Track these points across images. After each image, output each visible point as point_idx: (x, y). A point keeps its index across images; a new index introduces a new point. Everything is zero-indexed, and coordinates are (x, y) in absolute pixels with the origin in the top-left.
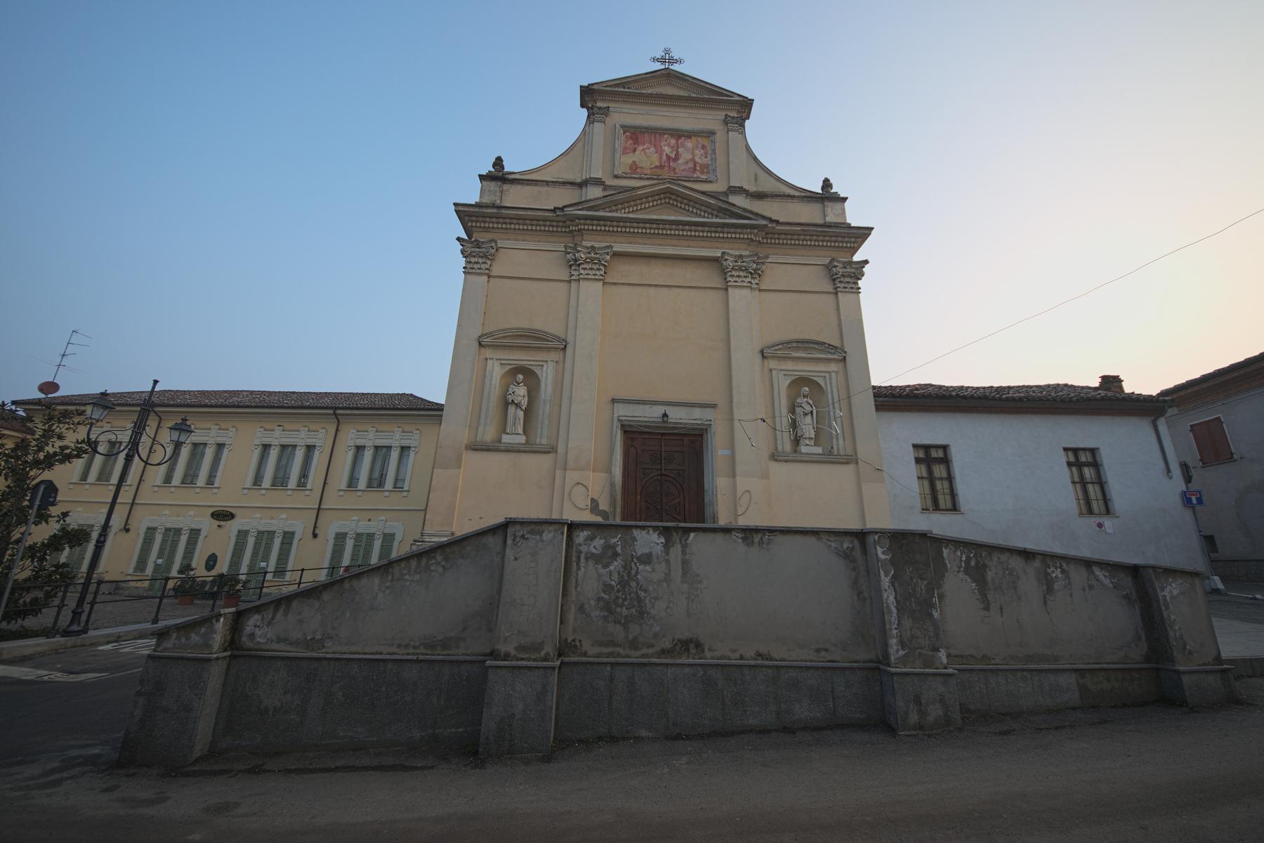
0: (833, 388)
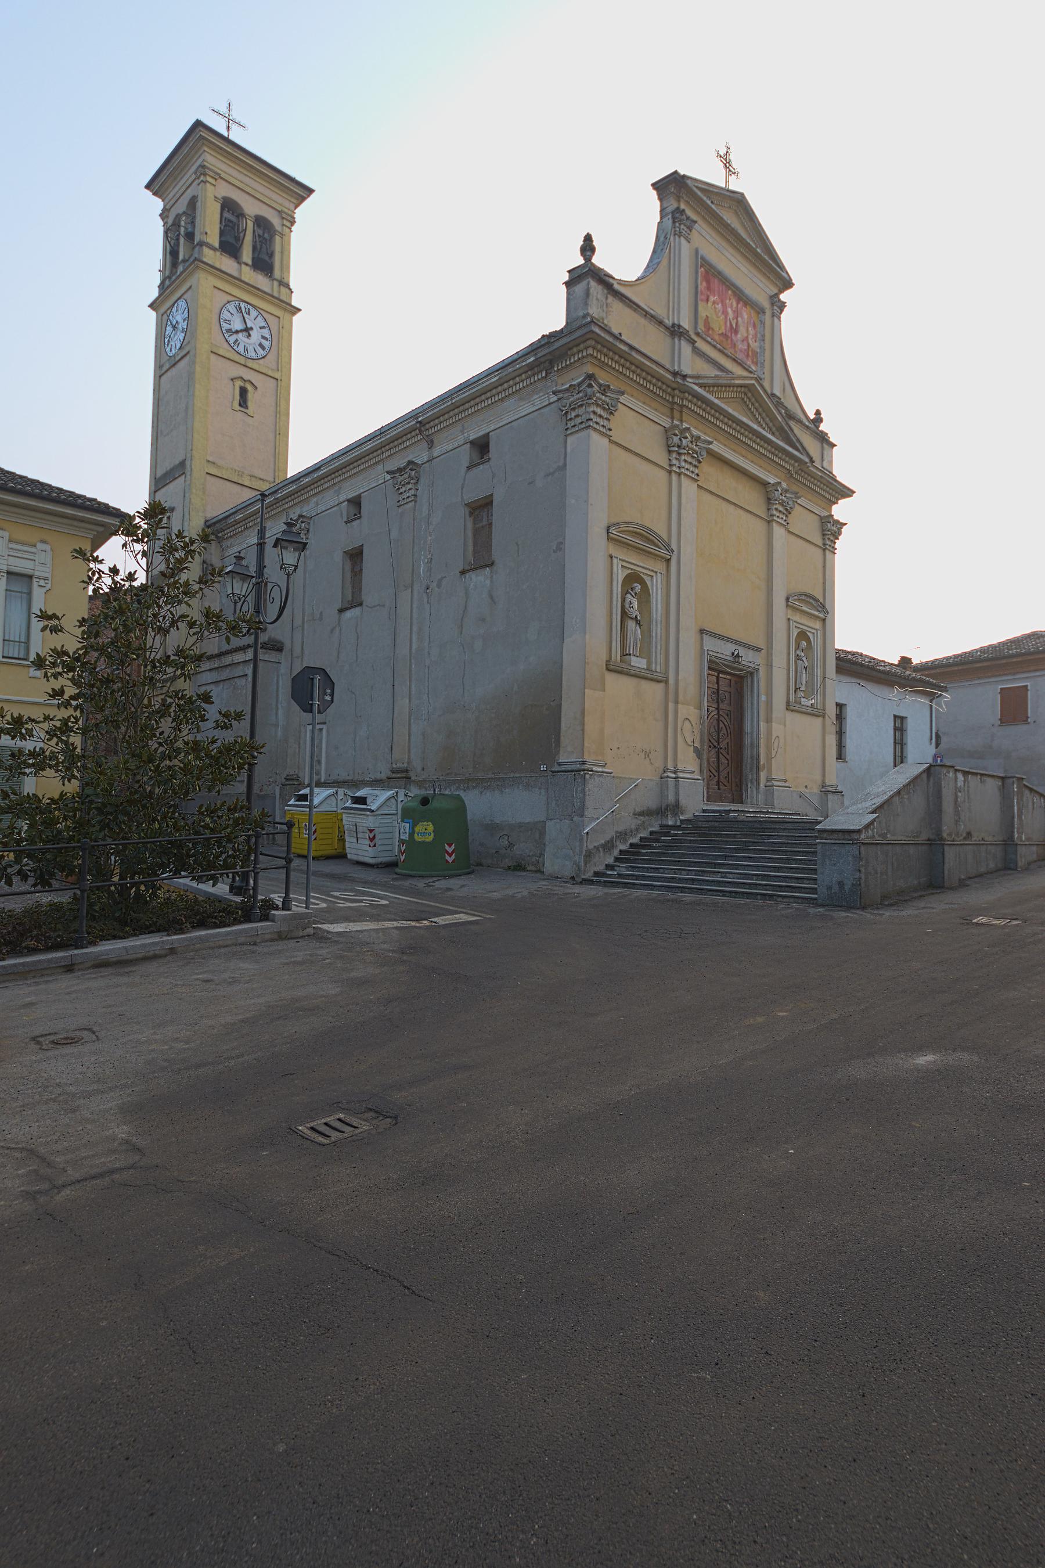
0: (817, 644)
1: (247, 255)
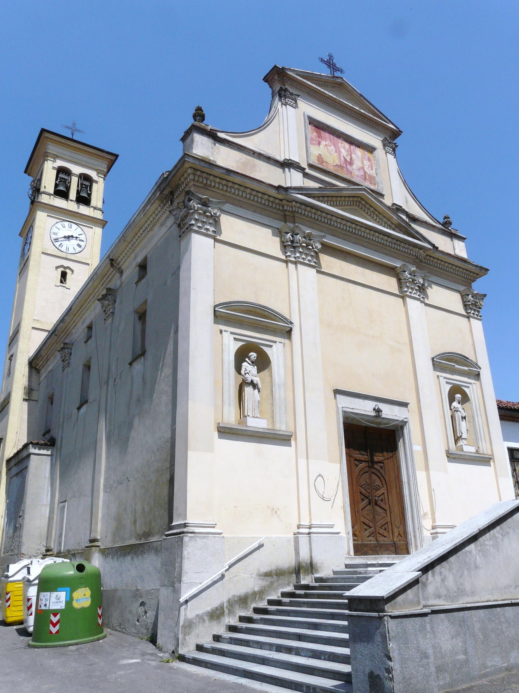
1: (73, 195)
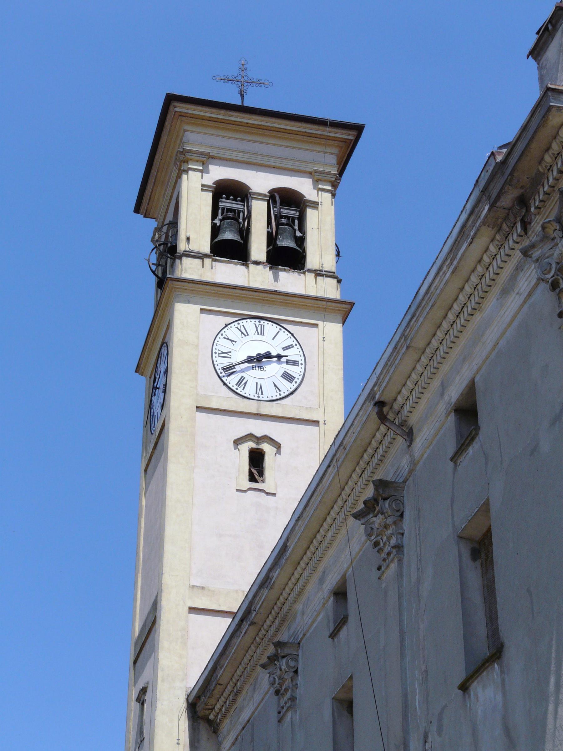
1: (258, 248)
